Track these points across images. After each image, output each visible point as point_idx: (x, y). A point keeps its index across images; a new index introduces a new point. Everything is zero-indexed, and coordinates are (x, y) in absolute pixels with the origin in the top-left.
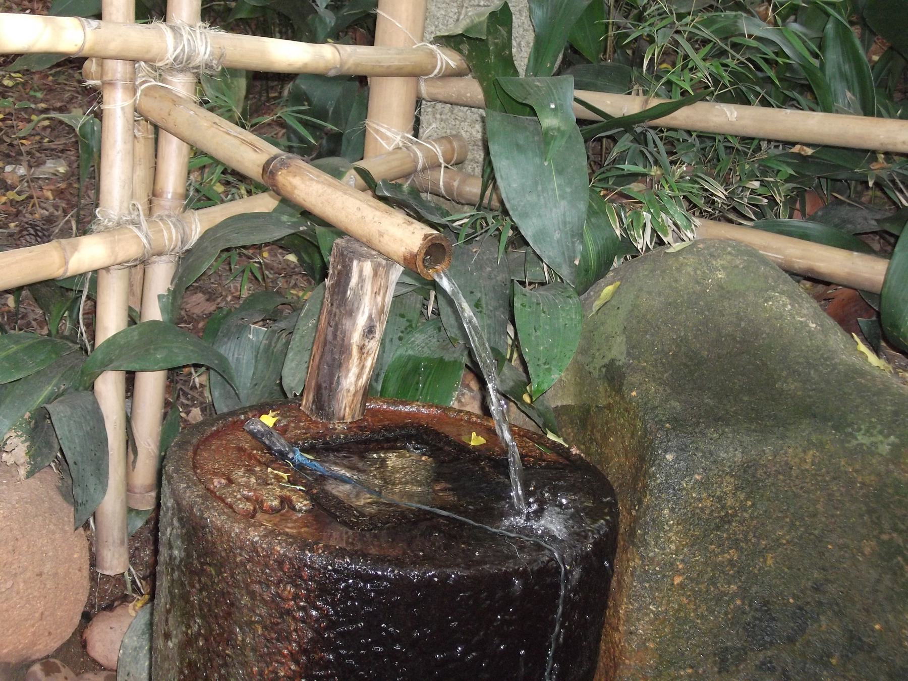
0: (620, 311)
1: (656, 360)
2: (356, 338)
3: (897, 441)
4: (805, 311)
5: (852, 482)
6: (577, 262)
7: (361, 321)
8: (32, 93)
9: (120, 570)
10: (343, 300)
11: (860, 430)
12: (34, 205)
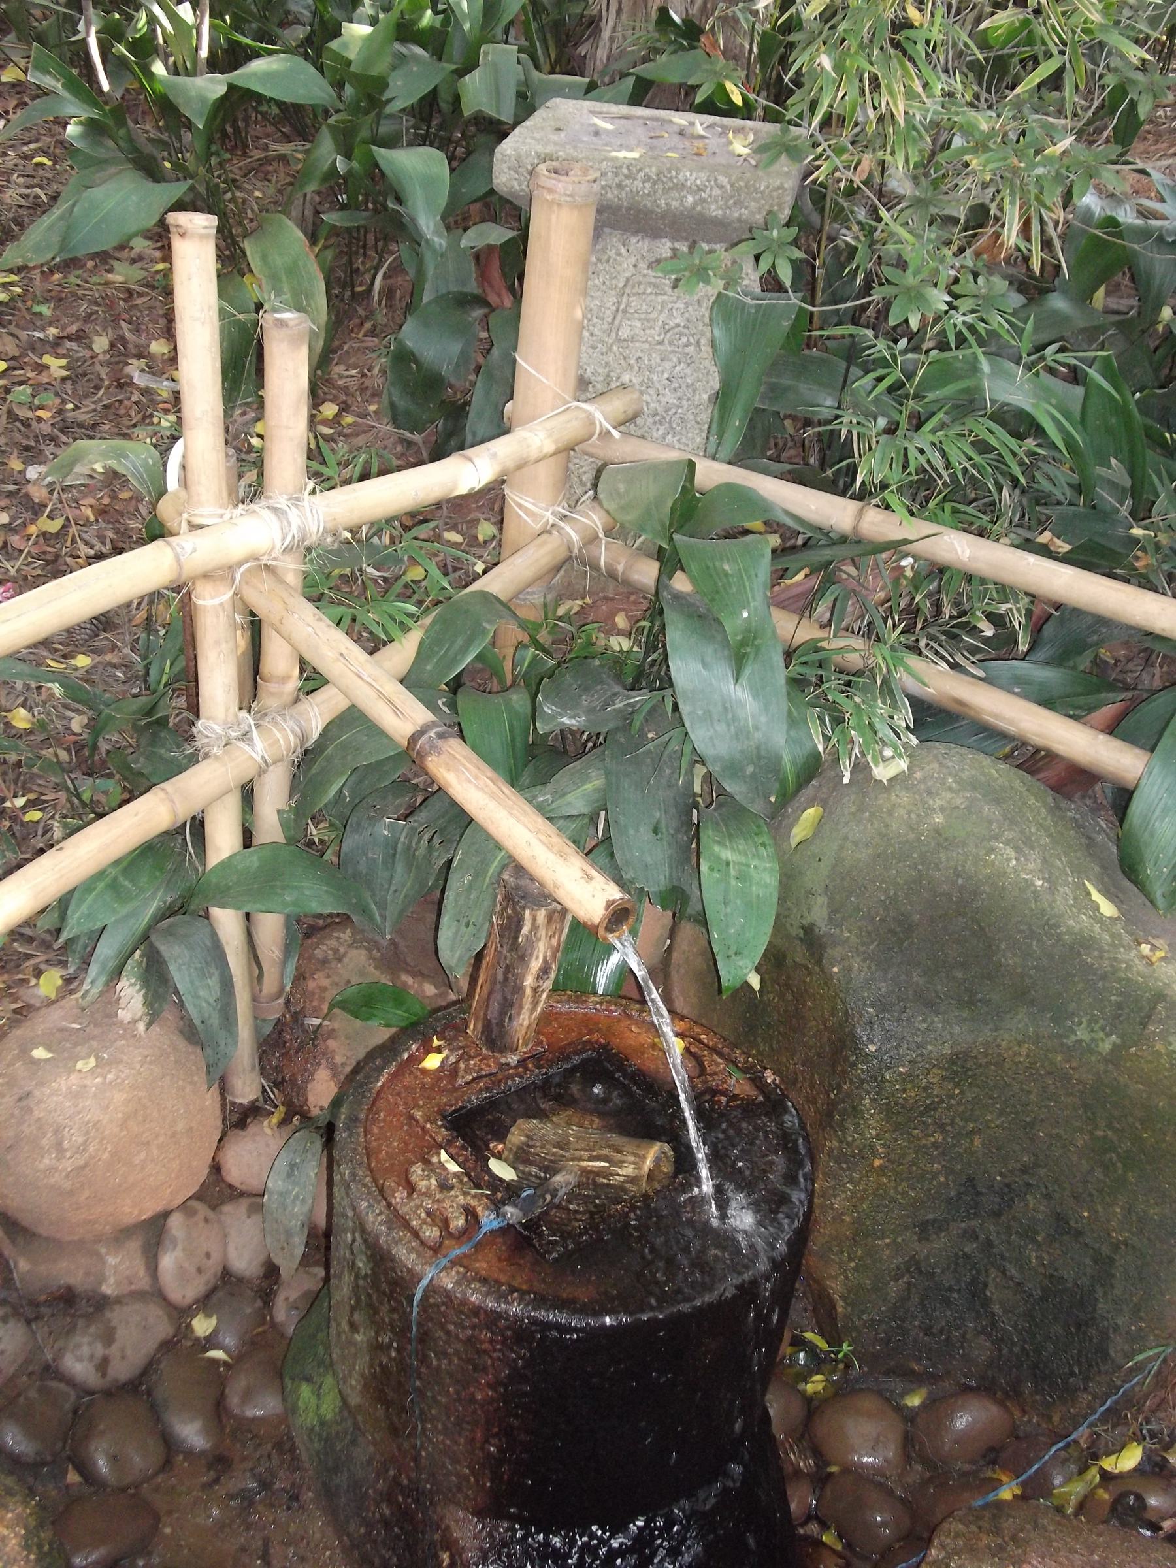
0: (822, 864)
1: (860, 928)
2: (529, 981)
3: (1118, 1041)
4: (1031, 866)
5: (1068, 1079)
6: (773, 799)
7: (535, 965)
8: (37, 309)
9: (252, 1097)
10: (514, 946)
11: (1080, 1023)
12: (73, 541)
